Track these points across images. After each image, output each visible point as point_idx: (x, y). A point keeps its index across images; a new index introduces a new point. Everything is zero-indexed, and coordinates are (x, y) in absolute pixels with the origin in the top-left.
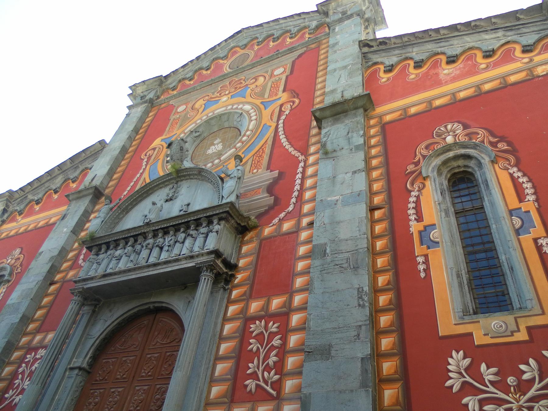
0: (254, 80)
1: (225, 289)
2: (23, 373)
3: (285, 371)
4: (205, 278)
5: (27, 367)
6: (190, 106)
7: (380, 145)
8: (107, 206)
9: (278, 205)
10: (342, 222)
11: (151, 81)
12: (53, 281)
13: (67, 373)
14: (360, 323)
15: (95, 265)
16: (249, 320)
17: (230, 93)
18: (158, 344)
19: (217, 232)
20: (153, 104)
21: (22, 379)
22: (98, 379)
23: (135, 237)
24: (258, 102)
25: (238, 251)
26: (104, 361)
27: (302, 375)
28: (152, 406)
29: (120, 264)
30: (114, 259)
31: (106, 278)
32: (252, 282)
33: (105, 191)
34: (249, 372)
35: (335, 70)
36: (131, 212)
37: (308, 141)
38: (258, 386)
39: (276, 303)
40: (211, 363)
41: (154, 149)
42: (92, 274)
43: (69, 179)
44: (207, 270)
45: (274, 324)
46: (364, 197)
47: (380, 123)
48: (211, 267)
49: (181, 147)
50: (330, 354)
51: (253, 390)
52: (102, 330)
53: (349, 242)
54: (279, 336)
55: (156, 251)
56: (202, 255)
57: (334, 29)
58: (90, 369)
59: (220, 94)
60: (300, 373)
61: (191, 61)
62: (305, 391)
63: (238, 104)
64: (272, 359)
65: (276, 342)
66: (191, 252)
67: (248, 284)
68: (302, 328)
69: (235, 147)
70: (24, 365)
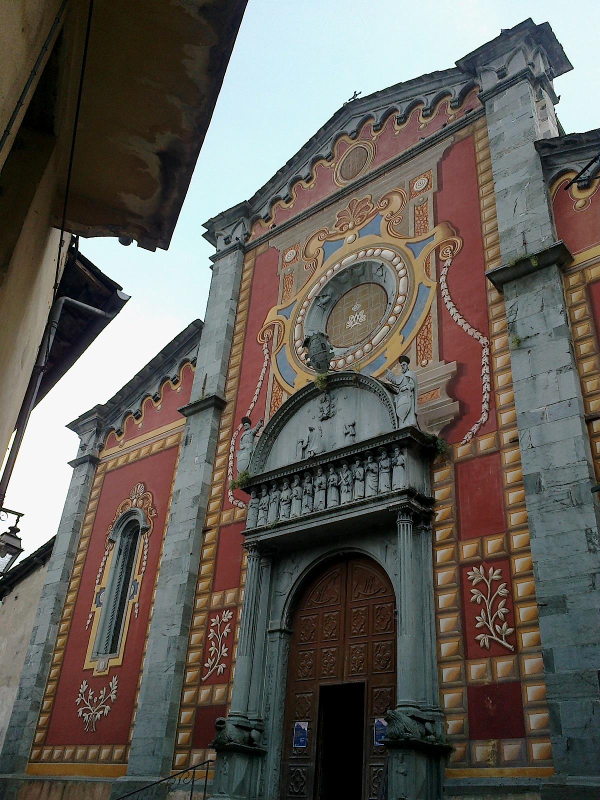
0: (386, 201)
2: (214, 638)
3: (518, 623)
4: (403, 525)
5: (216, 631)
6: (301, 249)
7: (586, 319)
8: (248, 431)
9: (465, 415)
10: (553, 443)
11: (233, 210)
12: (206, 527)
14: (594, 571)
15: (261, 512)
16: (464, 567)
17: (355, 226)
18: (361, 596)
19: (402, 465)
21: (217, 646)
22: (302, 639)
24: (401, 243)
25: (429, 477)
26: (303, 619)
27: (538, 627)
28: (376, 665)
29: (290, 509)
30: (283, 503)
31: (281, 528)
32: (457, 517)
33: (225, 396)
34: (478, 625)
35: (506, 192)
37: (487, 313)
38: (490, 640)
39: (492, 545)
40: (433, 618)
41: (272, 327)
42: (262, 523)
43: (168, 378)
44: (403, 515)
45: (494, 571)
46: (577, 409)
47: (584, 282)
48: (406, 510)
49: (322, 344)
50: (565, 606)
51: (487, 645)
53: (567, 471)
54: (504, 584)
55: (333, 493)
56: (393, 496)
57: (491, 106)
58: (290, 628)
59: (341, 229)
60: (536, 625)
62: (546, 646)
63: (373, 247)
64: (501, 611)
65: (502, 591)
66: (378, 491)
67: (451, 522)
68: (529, 573)
70: (212, 630)
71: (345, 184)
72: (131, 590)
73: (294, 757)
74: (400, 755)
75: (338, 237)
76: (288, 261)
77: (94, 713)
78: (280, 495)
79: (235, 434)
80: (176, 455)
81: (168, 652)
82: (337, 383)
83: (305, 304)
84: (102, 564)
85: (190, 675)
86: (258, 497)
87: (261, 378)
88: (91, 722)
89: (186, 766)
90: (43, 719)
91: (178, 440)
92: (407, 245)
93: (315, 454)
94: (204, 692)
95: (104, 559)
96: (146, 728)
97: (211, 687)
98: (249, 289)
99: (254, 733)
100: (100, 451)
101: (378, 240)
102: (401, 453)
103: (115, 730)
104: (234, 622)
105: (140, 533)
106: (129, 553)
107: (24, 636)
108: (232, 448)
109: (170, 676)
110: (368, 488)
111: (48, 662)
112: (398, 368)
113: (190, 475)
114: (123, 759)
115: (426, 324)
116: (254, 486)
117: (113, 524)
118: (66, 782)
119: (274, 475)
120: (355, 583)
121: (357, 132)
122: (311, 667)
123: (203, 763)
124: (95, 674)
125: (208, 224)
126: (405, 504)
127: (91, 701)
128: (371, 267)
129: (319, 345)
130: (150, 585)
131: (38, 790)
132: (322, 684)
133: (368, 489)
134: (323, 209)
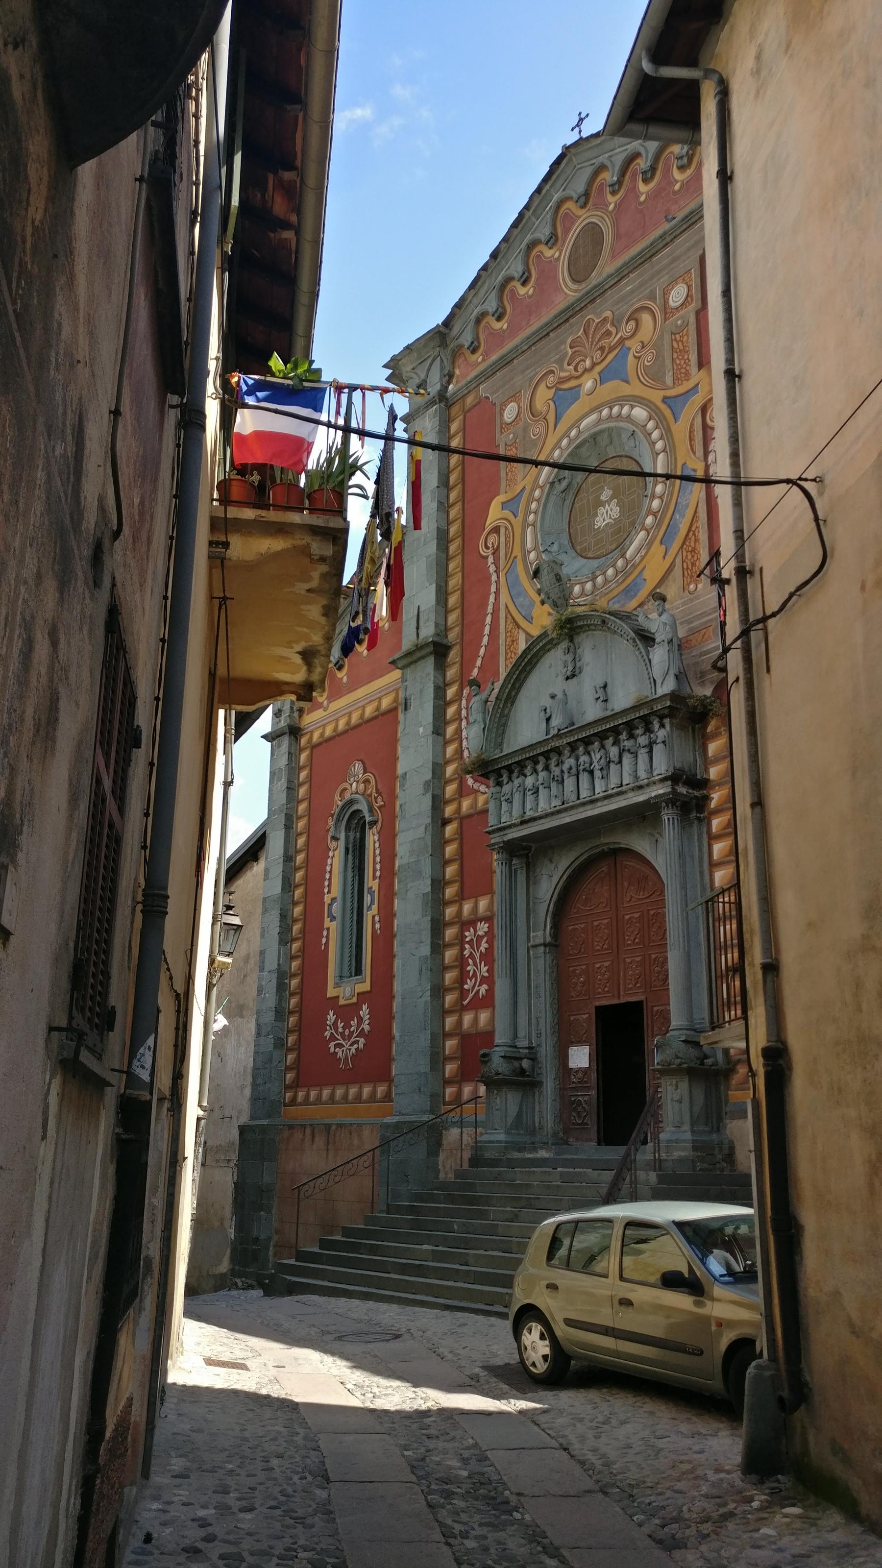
0: (632, 324)
1: (700, 820)
2: (471, 956)
13: (531, 953)
15: (504, 804)
17: (594, 365)
19: (664, 742)
20: (447, 399)
21: (475, 964)
23: (547, 755)
26: (571, 928)
29: (538, 803)
33: (446, 636)
36: (517, 701)
41: (496, 530)
48: (673, 800)
52: (552, 889)
55: (584, 778)
58: (556, 941)
59: (576, 369)
61: (484, 268)
63: (621, 400)
66: (636, 778)
69: (643, 528)
70: (467, 946)
71: (576, 291)
72: (367, 899)
73: (573, 1086)
74: (674, 1082)
75: (573, 383)
76: (509, 421)
77: (346, 1049)
78: (524, 782)
79: (465, 691)
80: (396, 722)
81: (420, 974)
82: (581, 627)
83: (537, 493)
84: (328, 868)
85: (449, 999)
86: (499, 784)
87: (490, 609)
88: (346, 1059)
89: (457, 1101)
90: (291, 1057)
91: (396, 700)
92: (665, 400)
93: (559, 730)
94: (468, 1018)
95: (329, 861)
96: (408, 1060)
97: (474, 1012)
98: (460, 468)
99: (525, 1064)
100: (300, 717)
101: (627, 390)
102: (662, 726)
103: (375, 1064)
104: (490, 934)
105: (367, 827)
106: (357, 852)
107: (249, 954)
108: (464, 712)
109: (426, 1002)
110: (625, 772)
111: (285, 991)
112: (652, 605)
113: (414, 756)
114: (388, 1097)
115: (693, 528)
116: (493, 771)
117: (332, 815)
118: (330, 1125)
119: (511, 758)
120: (626, 884)
121: (587, 194)
122: (584, 983)
123: (475, 1098)
124: (342, 1002)
125: (392, 364)
126: (669, 793)
127: (342, 1034)
128: (619, 436)
129: (552, 575)
130: (387, 896)
131: (301, 1136)
132: (598, 1004)
133: (625, 775)
134: (548, 334)
